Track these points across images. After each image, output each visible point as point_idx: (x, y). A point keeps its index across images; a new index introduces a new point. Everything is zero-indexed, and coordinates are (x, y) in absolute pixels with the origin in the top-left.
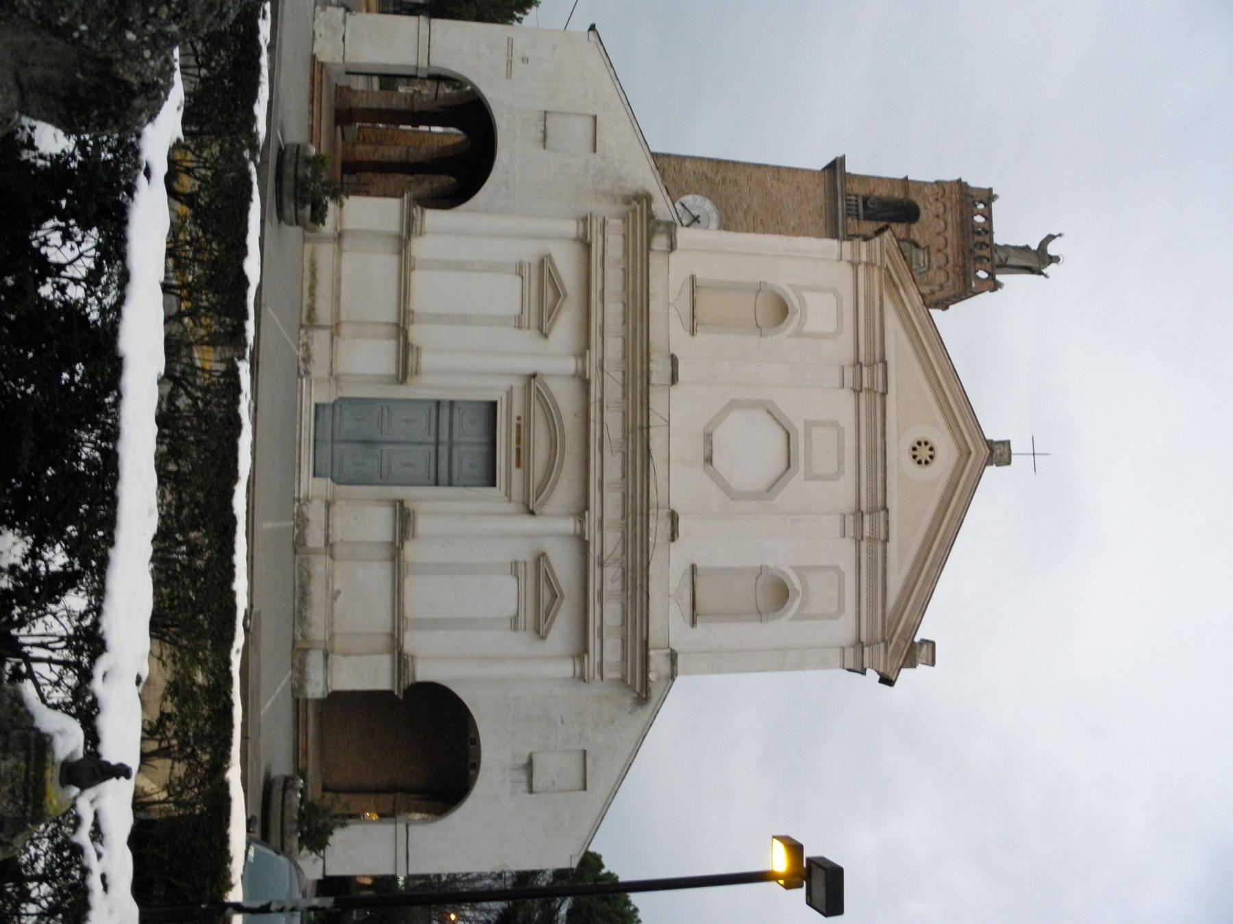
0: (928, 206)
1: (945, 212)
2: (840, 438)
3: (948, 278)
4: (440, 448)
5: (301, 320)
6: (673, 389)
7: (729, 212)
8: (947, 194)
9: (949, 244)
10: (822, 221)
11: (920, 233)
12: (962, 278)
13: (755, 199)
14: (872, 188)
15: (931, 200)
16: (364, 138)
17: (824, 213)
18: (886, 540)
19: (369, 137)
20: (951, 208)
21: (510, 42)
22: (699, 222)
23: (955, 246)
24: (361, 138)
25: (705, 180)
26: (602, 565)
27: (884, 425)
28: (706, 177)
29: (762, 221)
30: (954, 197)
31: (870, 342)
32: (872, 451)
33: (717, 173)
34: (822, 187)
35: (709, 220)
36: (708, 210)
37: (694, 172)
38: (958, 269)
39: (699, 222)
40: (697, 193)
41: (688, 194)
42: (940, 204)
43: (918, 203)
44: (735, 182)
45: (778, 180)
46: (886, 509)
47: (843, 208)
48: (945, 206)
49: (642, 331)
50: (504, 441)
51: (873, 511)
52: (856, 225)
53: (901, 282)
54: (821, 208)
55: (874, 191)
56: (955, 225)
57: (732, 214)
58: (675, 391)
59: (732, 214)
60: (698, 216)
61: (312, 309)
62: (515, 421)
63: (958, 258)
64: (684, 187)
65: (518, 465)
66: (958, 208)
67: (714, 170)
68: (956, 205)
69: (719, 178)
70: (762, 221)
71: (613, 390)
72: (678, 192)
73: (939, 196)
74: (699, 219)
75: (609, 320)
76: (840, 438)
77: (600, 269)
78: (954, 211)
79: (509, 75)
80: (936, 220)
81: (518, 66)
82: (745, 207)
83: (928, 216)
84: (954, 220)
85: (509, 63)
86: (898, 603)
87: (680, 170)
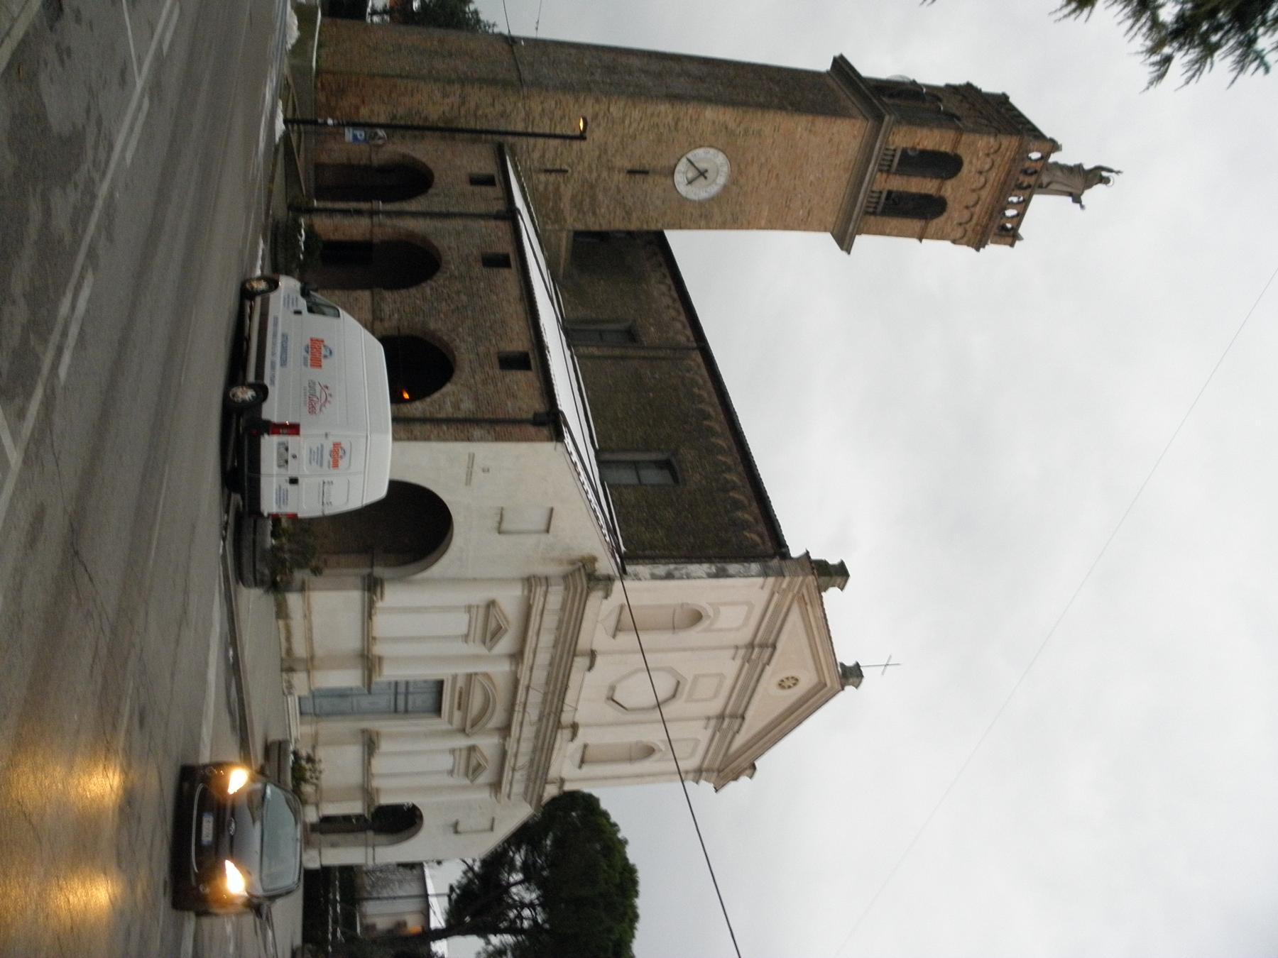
0: (974, 161)
1: (990, 168)
2: (720, 685)
3: (964, 236)
4: (399, 697)
5: (281, 654)
6: (588, 674)
7: (742, 166)
8: (1001, 150)
9: (980, 203)
10: (847, 176)
11: (953, 189)
12: (979, 237)
13: (776, 152)
14: (917, 140)
15: (981, 154)
16: (322, 85)
17: (851, 167)
18: (738, 732)
19: (329, 84)
20: (999, 166)
21: (472, 458)
22: (706, 178)
23: (986, 205)
24: (319, 85)
25: (724, 130)
26: (514, 770)
27: (760, 676)
28: (726, 128)
29: (777, 175)
30: (1008, 153)
31: (769, 630)
32: (744, 688)
33: (740, 123)
34: (859, 139)
35: (718, 174)
36: (719, 163)
37: (714, 123)
38: (979, 227)
39: (706, 178)
40: (711, 146)
41: (701, 146)
42: (989, 160)
43: (964, 158)
44: (759, 134)
45: (810, 131)
46: (743, 718)
47: (862, 204)
48: (993, 164)
49: (579, 608)
50: (449, 689)
51: (733, 716)
52: (883, 180)
53: (811, 602)
54: (850, 162)
55: (918, 144)
56: (995, 184)
57: (746, 168)
58: (589, 675)
59: (746, 168)
60: (706, 171)
61: (289, 651)
62: (457, 690)
63: (983, 218)
64: (697, 139)
65: (459, 708)
66: (1007, 166)
67: (738, 120)
68: (1007, 163)
69: (741, 128)
70: (777, 175)
71: (535, 698)
72: (690, 144)
73: (992, 150)
74: (706, 175)
75: (549, 606)
76: (720, 685)
77: (538, 617)
78: (1001, 169)
79: (468, 481)
80: (977, 176)
81: (478, 475)
82: (763, 160)
83: (970, 172)
84: (997, 178)
85: (469, 475)
86: (736, 752)
87: (697, 120)
